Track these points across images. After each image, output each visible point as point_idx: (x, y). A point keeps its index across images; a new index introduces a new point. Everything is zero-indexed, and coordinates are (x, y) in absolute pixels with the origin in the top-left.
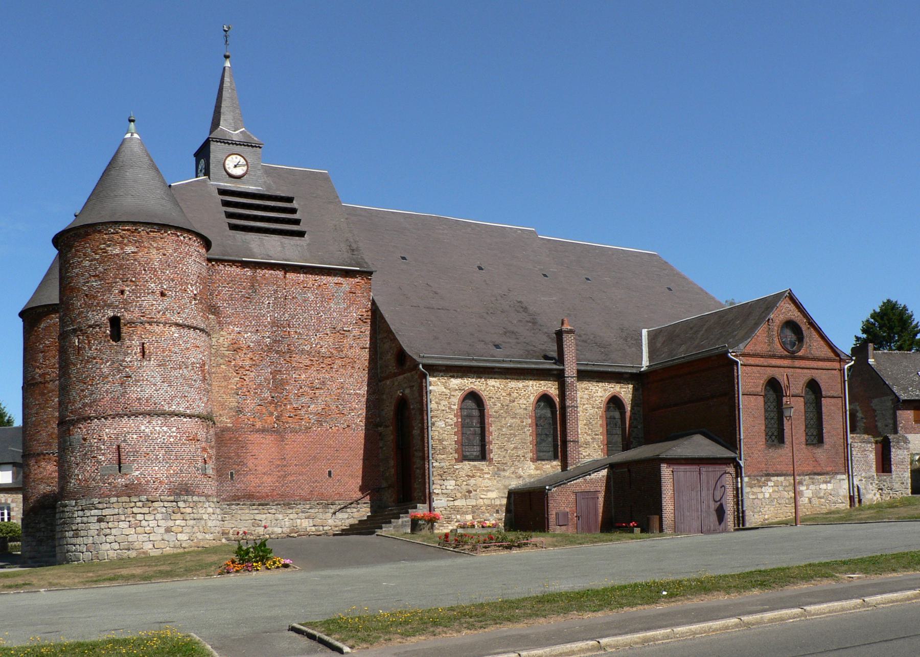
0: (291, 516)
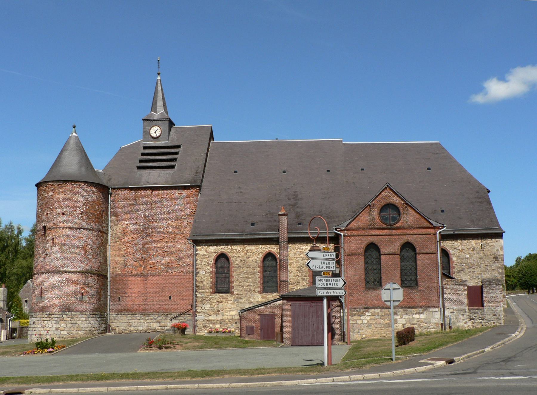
0: (148, 321)
